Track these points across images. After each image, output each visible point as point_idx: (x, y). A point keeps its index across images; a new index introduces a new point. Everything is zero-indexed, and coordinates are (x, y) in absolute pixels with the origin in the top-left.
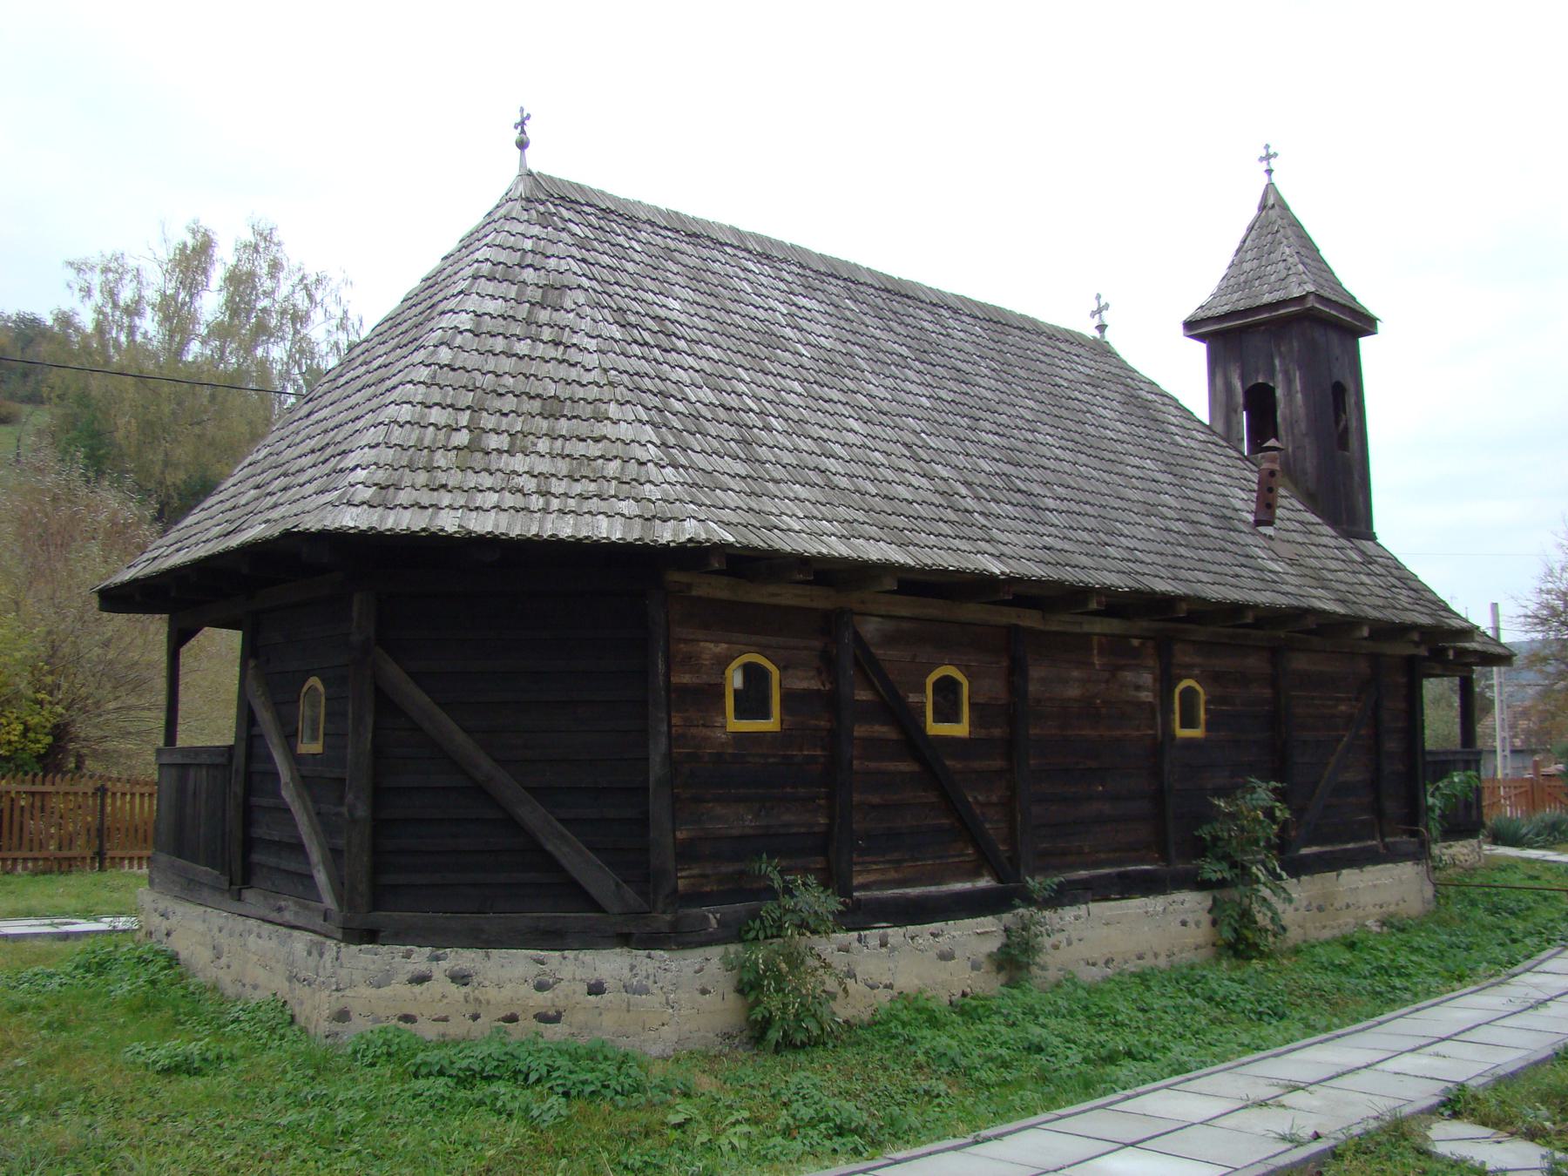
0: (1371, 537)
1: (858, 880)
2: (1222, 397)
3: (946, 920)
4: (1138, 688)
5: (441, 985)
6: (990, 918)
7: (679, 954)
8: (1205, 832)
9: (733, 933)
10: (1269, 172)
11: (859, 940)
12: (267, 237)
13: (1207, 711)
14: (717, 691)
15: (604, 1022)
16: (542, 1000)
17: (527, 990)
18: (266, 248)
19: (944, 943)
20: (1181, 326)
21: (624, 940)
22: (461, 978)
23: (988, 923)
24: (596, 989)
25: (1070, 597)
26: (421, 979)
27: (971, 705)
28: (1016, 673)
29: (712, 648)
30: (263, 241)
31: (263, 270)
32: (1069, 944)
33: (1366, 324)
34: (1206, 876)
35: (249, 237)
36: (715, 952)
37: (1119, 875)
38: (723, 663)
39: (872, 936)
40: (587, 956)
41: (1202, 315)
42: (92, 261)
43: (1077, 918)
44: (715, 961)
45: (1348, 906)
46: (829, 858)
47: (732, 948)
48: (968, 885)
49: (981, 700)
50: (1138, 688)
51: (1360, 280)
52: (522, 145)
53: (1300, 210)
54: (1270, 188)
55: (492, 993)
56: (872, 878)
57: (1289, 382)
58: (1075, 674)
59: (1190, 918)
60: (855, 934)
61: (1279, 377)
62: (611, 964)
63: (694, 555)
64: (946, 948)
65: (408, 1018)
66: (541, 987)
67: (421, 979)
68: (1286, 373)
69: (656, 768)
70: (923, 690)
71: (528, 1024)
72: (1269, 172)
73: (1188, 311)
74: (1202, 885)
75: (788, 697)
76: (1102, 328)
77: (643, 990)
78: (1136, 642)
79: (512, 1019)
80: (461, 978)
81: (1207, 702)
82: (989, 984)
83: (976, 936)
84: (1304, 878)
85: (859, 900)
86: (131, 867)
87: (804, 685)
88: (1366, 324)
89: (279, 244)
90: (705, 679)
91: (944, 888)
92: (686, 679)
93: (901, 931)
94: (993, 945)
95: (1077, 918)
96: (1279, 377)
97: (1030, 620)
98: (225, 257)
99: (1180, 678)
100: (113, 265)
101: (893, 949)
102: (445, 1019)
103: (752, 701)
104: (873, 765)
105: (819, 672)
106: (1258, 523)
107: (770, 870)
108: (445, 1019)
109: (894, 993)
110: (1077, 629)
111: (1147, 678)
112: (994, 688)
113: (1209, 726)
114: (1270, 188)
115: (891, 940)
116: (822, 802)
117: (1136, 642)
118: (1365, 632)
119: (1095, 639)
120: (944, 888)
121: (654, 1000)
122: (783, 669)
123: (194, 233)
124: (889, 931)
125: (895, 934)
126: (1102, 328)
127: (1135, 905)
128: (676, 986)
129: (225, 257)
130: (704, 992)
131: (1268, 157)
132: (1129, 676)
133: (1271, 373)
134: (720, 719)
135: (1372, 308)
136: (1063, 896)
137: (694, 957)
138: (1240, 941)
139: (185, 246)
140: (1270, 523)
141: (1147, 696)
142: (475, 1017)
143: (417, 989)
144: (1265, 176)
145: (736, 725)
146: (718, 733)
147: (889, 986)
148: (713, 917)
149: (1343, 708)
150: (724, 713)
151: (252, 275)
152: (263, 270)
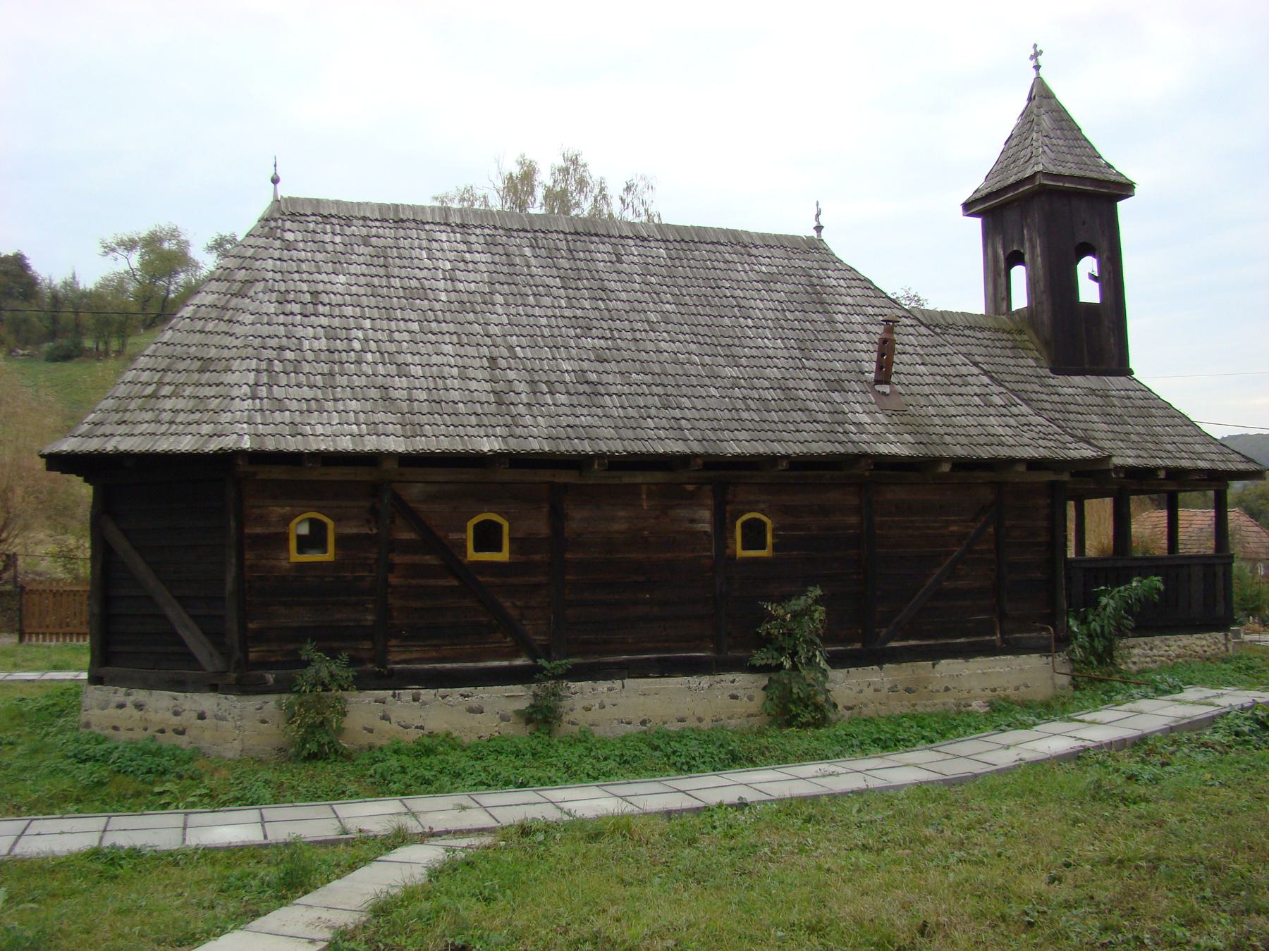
0: (1130, 372)
1: (391, 657)
2: (991, 263)
3: (476, 686)
4: (692, 521)
5: (130, 710)
6: (519, 686)
7: (243, 698)
8: (762, 630)
9: (282, 687)
10: (1037, 67)
11: (394, 696)
12: (574, 161)
13: (774, 536)
14: (285, 539)
15: (203, 735)
16: (175, 721)
17: (169, 715)
18: (575, 170)
19: (473, 702)
20: (961, 208)
21: (214, 688)
22: (139, 706)
23: (517, 689)
24: (202, 716)
25: (578, 462)
26: (121, 706)
27: (512, 540)
28: (557, 516)
29: (278, 511)
30: (572, 167)
31: (572, 186)
32: (602, 707)
33: (1125, 189)
34: (753, 662)
35: (562, 164)
36: (272, 700)
37: (658, 660)
38: (287, 520)
39: (406, 694)
40: (197, 696)
41: (978, 195)
42: (452, 194)
43: (610, 689)
44: (272, 704)
45: (947, 689)
46: (330, 639)
47: (285, 696)
48: (505, 663)
49: (519, 535)
50: (692, 521)
51: (1118, 153)
52: (275, 181)
53: (1065, 96)
54: (1039, 82)
55: (152, 716)
56: (414, 656)
57: (1033, 248)
58: (621, 514)
59: (740, 693)
60: (391, 692)
61: (1027, 245)
62: (207, 702)
63: (259, 457)
64: (475, 705)
65: (116, 728)
66: (176, 713)
67: (121, 706)
68: (1031, 240)
69: (230, 585)
70: (464, 530)
71: (170, 734)
72: (1037, 67)
73: (967, 194)
74: (753, 669)
75: (340, 540)
76: (819, 229)
77: (223, 719)
78: (690, 488)
79: (162, 731)
80: (139, 706)
81: (774, 530)
82: (518, 732)
83: (518, 697)
84: (886, 666)
85: (392, 670)
86: (37, 640)
87: (354, 531)
88: (1125, 189)
89: (585, 166)
90: (272, 530)
91: (481, 665)
92: (258, 530)
93: (432, 692)
94: (523, 705)
95: (610, 689)
96: (1027, 245)
97: (564, 477)
98: (544, 178)
99: (743, 513)
100: (466, 196)
101: (424, 703)
102: (131, 730)
103: (314, 540)
104: (414, 582)
105: (368, 521)
106: (877, 382)
107: (308, 650)
108: (131, 730)
109: (426, 732)
110: (617, 481)
111: (706, 514)
112: (539, 525)
113: (776, 547)
114: (1039, 82)
115: (422, 698)
116: (370, 606)
117: (690, 488)
118: (946, 468)
119: (644, 488)
120: (481, 665)
121: (229, 725)
122: (337, 520)
123: (522, 164)
124: (422, 691)
125: (427, 694)
126: (819, 229)
127: (676, 683)
128: (242, 718)
129: (544, 178)
130: (264, 722)
131: (1036, 55)
132: (683, 513)
133: (1022, 243)
134: (283, 555)
135: (1130, 173)
136: (577, 674)
137: (252, 702)
138: (542, 717)
139: (528, 175)
140: (887, 382)
141: (707, 527)
142: (146, 729)
143: (120, 711)
144: (1034, 71)
145: (295, 557)
146: (284, 563)
147: (422, 728)
148: (270, 677)
149: (954, 528)
150: (287, 550)
151: (564, 192)
152: (572, 186)
